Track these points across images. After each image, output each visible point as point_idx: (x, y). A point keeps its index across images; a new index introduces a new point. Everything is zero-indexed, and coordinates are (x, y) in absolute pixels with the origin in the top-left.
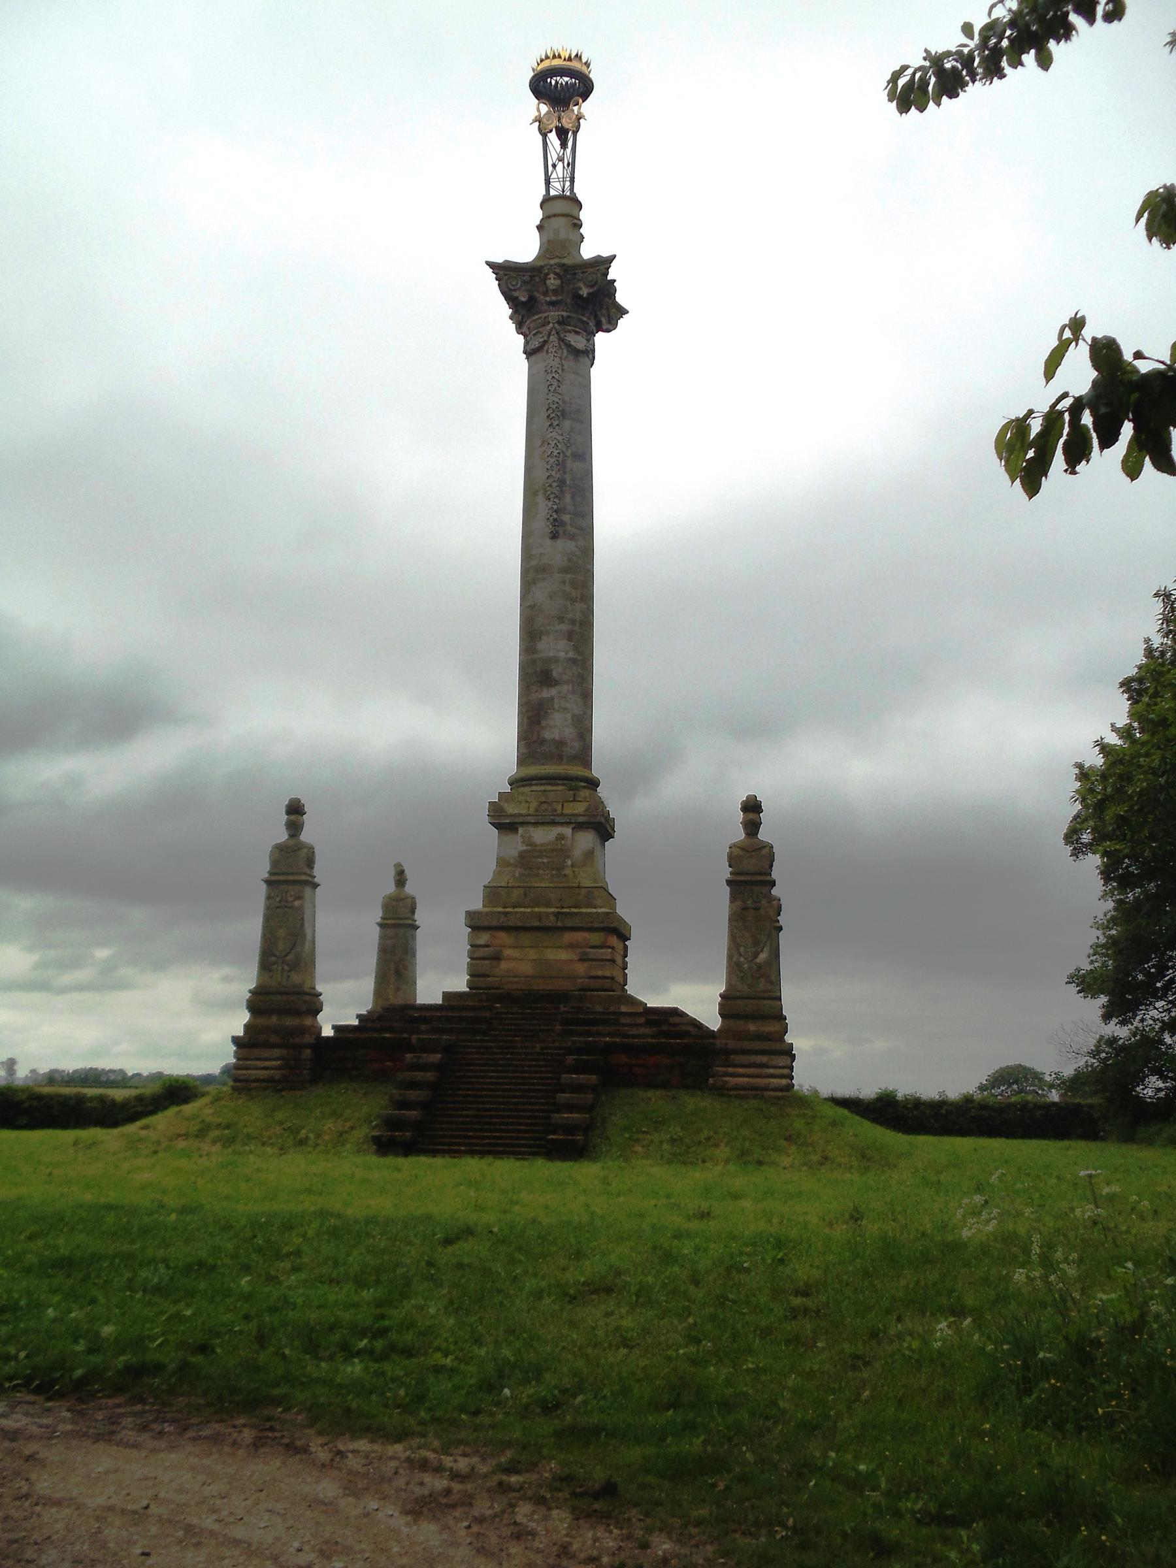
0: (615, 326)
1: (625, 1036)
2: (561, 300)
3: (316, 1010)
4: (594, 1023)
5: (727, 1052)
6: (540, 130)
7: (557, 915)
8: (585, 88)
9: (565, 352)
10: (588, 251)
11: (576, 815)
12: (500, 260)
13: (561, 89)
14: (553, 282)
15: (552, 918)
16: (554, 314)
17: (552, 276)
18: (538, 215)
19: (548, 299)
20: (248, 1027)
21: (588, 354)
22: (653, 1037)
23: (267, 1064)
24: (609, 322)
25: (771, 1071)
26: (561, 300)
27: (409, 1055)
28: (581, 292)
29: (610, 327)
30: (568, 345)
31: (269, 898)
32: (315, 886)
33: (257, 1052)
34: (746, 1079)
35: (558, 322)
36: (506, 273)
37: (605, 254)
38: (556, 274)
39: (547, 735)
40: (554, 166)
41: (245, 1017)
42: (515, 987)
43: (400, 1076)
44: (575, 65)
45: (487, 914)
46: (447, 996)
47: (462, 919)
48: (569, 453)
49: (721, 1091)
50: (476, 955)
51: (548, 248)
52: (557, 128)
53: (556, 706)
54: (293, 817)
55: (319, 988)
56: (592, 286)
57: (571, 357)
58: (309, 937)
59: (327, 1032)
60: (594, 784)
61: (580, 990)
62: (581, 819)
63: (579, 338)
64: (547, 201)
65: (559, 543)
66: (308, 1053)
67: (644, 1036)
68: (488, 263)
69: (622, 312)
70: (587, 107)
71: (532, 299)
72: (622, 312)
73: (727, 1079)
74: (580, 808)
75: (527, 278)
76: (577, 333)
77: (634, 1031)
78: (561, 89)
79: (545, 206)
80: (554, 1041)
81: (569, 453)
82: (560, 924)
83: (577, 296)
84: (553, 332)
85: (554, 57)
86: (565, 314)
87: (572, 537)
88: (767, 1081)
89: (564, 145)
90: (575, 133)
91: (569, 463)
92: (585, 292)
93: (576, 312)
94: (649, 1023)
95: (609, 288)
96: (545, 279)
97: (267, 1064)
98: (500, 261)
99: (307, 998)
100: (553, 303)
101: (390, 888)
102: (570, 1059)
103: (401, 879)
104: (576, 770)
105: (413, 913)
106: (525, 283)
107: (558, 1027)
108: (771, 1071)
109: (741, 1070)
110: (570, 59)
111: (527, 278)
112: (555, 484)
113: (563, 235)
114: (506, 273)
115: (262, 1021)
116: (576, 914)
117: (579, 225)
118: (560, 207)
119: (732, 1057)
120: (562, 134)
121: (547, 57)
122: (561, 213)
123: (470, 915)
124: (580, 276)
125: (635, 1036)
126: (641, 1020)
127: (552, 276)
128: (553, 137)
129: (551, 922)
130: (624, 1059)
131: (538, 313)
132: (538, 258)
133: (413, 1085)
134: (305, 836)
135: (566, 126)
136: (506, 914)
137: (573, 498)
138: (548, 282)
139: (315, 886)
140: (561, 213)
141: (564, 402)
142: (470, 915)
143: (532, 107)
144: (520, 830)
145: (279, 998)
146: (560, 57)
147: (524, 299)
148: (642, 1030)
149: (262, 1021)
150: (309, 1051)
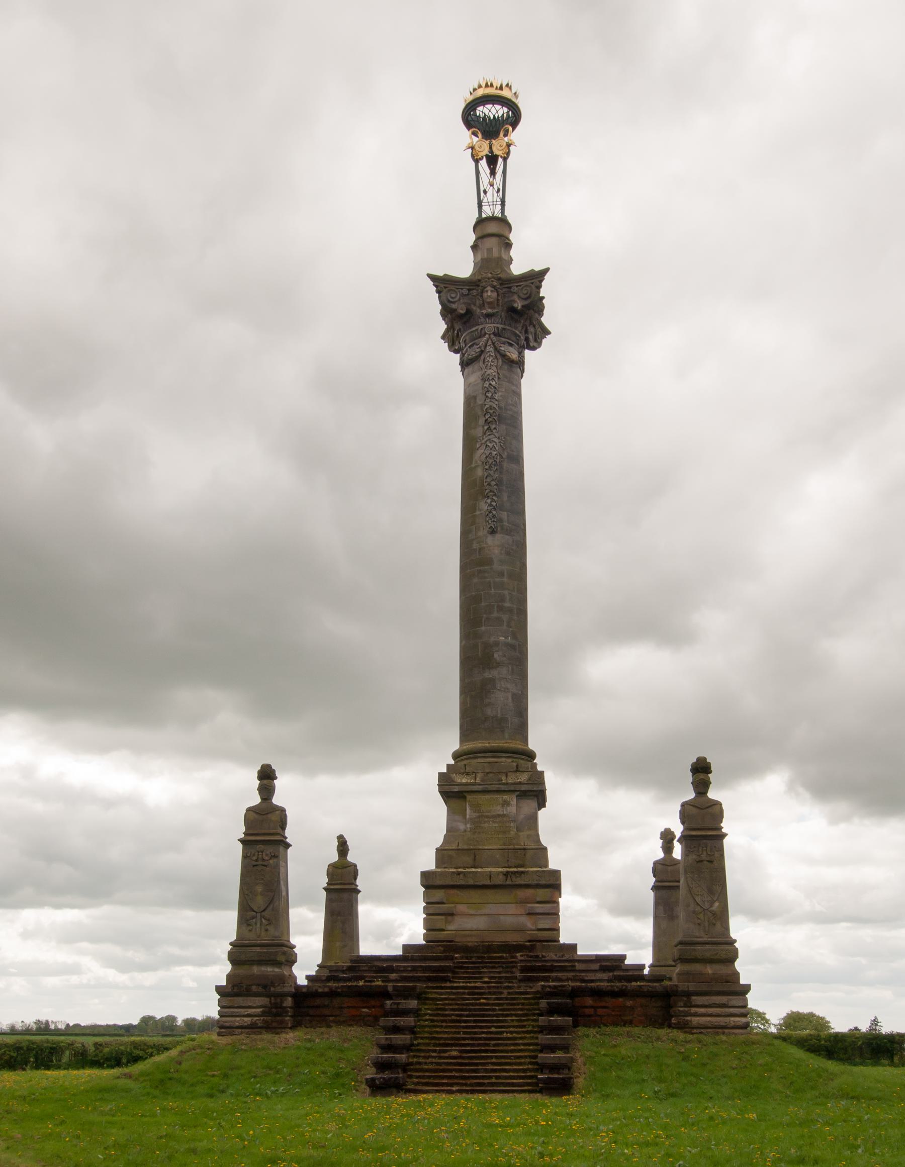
0: (540, 344)
1: (583, 981)
2: (493, 313)
3: (291, 960)
4: (551, 969)
5: (689, 994)
6: (473, 156)
7: (506, 874)
8: (515, 118)
9: (500, 361)
10: (518, 268)
11: (520, 783)
12: (440, 274)
13: (491, 121)
14: (490, 294)
15: (501, 876)
16: (490, 327)
17: (489, 288)
18: (472, 238)
19: (484, 312)
20: (229, 977)
21: (519, 364)
22: (609, 981)
23: (250, 1011)
24: (536, 340)
25: (732, 1010)
26: (493, 313)
27: (388, 1002)
28: (515, 305)
29: (535, 344)
30: (504, 356)
31: (245, 857)
32: (288, 846)
33: (240, 1000)
34: (709, 1019)
35: (494, 334)
36: (443, 284)
37: (537, 269)
38: (494, 287)
39: (489, 712)
40: (485, 192)
41: (228, 967)
42: (469, 939)
43: (383, 1021)
44: (506, 93)
45: (441, 874)
46: (406, 947)
47: (418, 879)
48: (505, 455)
49: (684, 1027)
50: (431, 912)
51: (481, 265)
52: (487, 156)
53: (498, 686)
54: (265, 782)
55: (293, 940)
56: (526, 299)
57: (506, 367)
58: (284, 893)
59: (302, 981)
60: (531, 756)
61: (529, 941)
62: (524, 788)
63: (511, 349)
64: (481, 222)
65: (498, 536)
66: (289, 1002)
67: (600, 980)
68: (430, 276)
69: (546, 332)
70: (515, 136)
71: (469, 312)
72: (546, 332)
73: (689, 1018)
74: (523, 778)
75: (465, 292)
76: (511, 345)
77: (591, 976)
78: (491, 121)
79: (478, 229)
80: (519, 987)
81: (505, 455)
82: (509, 882)
83: (512, 310)
84: (490, 343)
85: (487, 85)
86: (500, 326)
87: (508, 532)
88: (727, 1019)
89: (493, 173)
90: (505, 159)
91: (505, 465)
92: (519, 305)
93: (510, 325)
94: (604, 969)
95: (535, 306)
96: (482, 292)
97: (250, 1011)
98: (441, 274)
99: (285, 949)
100: (488, 316)
101: (334, 857)
102: (543, 1003)
103: (343, 846)
104: (516, 745)
105: (355, 879)
106: (463, 295)
107: (518, 974)
108: (732, 1010)
109: (702, 1010)
110: (501, 88)
111: (465, 292)
112: (493, 483)
113: (495, 253)
114: (443, 284)
115: (243, 971)
116: (522, 872)
117: (509, 245)
118: (492, 228)
119: (694, 998)
120: (492, 160)
121: (480, 86)
122: (492, 232)
123: (425, 875)
124: (515, 289)
125: (592, 981)
126: (596, 966)
127: (489, 288)
128: (483, 163)
129: (500, 880)
130: (589, 1001)
131: (473, 326)
132: (471, 275)
133: (396, 1029)
134: (277, 800)
135: (496, 152)
136: (459, 874)
137: (509, 497)
138: (485, 295)
139: (288, 846)
140: (492, 232)
141: (500, 408)
142: (425, 875)
143: (465, 137)
144: (469, 797)
145: (258, 949)
146: (492, 85)
147: (462, 312)
148: (600, 975)
149: (243, 971)
150: (290, 999)
